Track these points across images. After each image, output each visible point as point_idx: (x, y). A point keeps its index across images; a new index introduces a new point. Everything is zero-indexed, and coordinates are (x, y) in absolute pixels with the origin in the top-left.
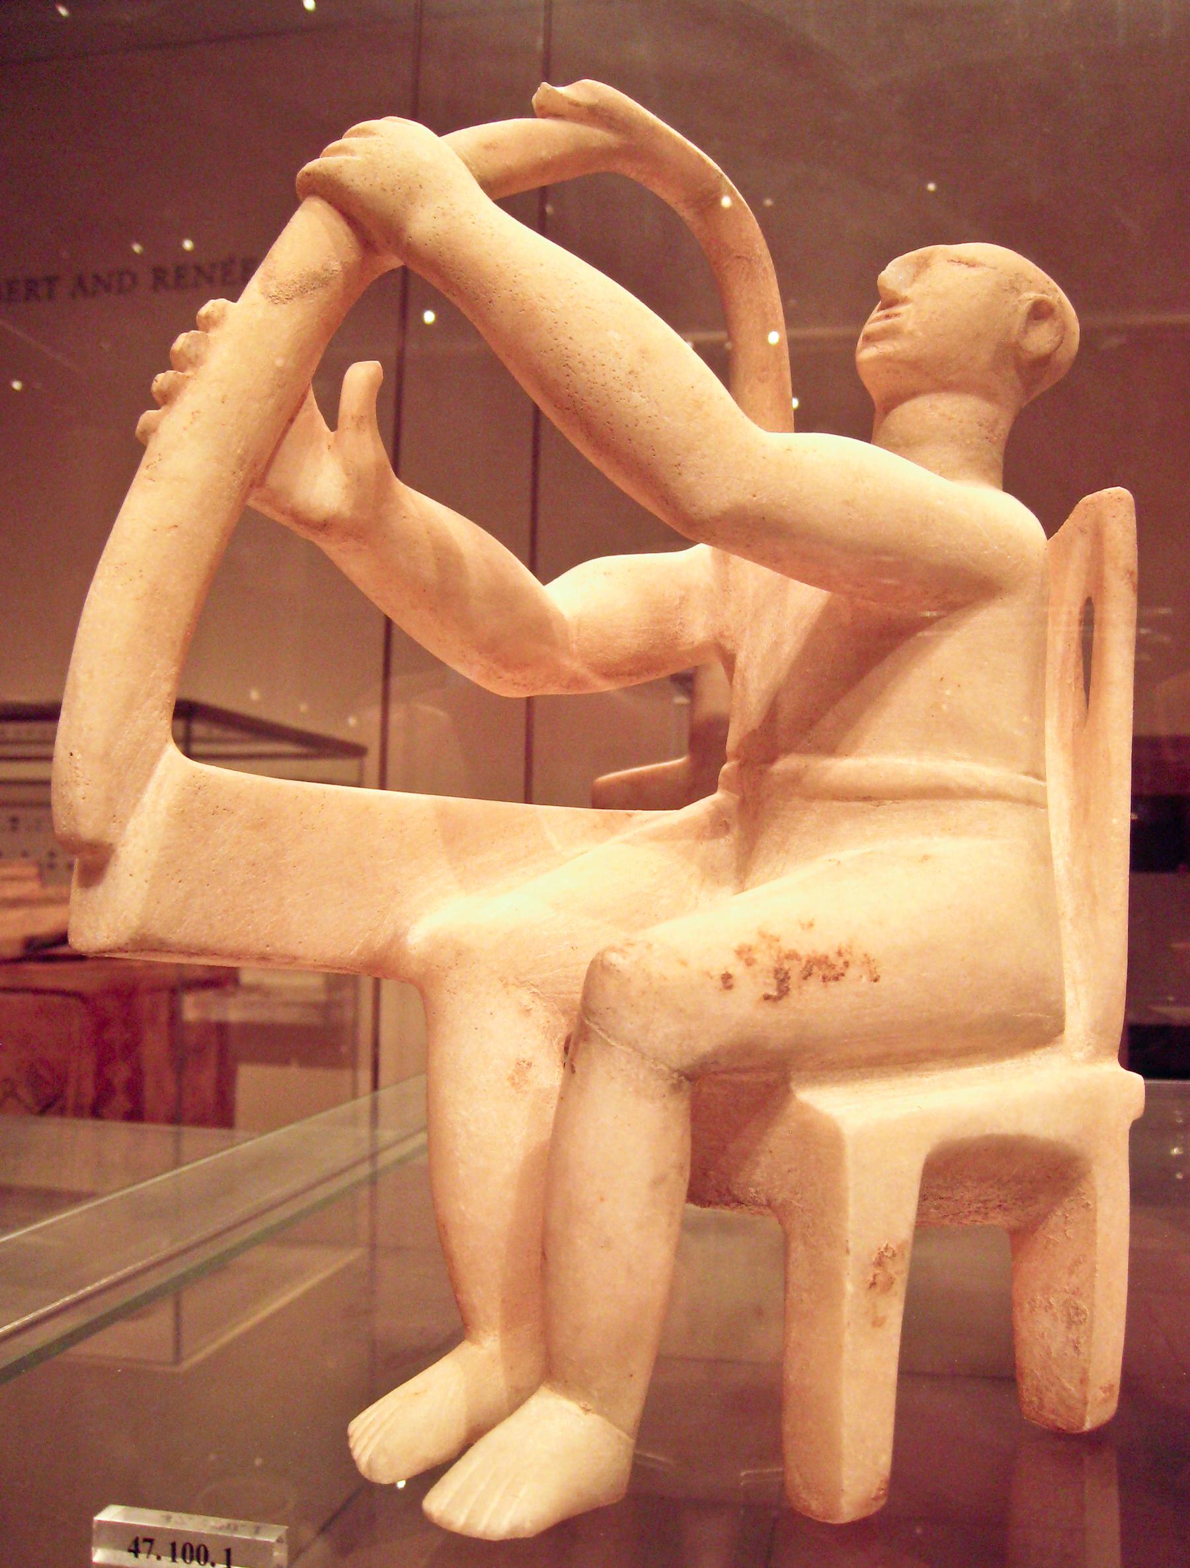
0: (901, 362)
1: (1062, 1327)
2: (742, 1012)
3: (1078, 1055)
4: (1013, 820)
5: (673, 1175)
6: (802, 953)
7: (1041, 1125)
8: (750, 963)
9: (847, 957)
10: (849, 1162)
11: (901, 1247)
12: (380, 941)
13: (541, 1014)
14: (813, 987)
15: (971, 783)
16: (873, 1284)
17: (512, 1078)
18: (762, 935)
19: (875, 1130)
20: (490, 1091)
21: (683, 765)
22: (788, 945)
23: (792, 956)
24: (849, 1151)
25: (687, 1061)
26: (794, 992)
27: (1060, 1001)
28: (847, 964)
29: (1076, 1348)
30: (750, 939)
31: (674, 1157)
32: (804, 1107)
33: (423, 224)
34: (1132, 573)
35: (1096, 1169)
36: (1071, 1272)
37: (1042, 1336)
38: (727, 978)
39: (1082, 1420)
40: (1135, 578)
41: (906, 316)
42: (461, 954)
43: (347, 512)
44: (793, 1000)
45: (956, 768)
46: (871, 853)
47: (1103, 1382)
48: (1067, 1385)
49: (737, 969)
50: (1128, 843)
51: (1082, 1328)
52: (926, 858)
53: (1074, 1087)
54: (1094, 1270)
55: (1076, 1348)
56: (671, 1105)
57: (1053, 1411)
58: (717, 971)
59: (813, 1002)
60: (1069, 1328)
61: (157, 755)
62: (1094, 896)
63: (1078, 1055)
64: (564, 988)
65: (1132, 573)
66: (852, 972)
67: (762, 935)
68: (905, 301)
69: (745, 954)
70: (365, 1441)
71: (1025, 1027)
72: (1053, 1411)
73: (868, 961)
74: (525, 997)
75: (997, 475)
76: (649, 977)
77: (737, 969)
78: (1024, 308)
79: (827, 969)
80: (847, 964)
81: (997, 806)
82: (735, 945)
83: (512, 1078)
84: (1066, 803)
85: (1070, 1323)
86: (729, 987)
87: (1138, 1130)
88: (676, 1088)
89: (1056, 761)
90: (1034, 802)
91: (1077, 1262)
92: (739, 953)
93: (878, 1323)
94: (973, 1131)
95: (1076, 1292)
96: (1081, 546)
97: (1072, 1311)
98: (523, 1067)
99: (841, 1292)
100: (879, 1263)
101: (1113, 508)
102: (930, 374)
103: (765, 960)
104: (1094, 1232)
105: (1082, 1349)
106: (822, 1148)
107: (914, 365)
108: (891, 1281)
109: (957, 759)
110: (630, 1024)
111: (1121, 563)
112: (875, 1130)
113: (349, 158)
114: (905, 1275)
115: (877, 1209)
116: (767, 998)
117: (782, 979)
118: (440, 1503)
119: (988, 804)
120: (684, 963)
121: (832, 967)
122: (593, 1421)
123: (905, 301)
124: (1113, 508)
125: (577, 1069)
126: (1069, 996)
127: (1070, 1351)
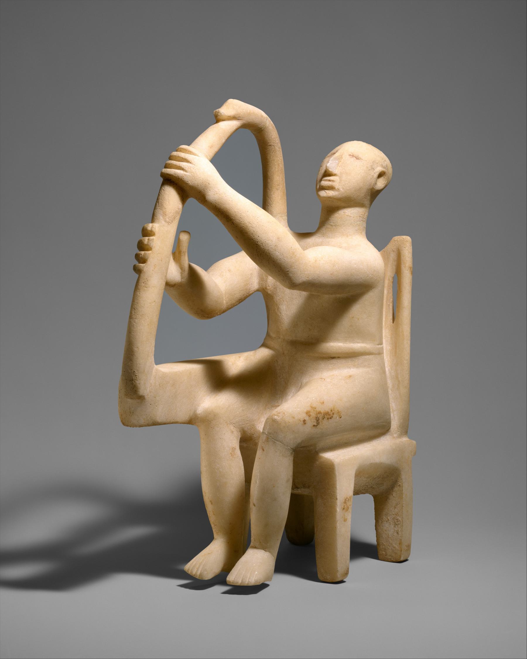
0: (335, 199)
1: (393, 526)
2: (308, 429)
3: (395, 435)
6: (322, 412)
7: (385, 459)
8: (309, 416)
9: (333, 412)
11: (350, 497)
16: (344, 509)
17: (231, 453)
18: (312, 407)
19: (346, 461)
21: (337, 340)
22: (318, 409)
23: (320, 413)
24: (336, 468)
26: (320, 423)
27: (390, 419)
28: (333, 414)
29: (397, 533)
30: (309, 409)
32: (322, 457)
35: (402, 473)
36: (395, 508)
37: (386, 531)
38: (304, 421)
39: (400, 557)
40: (412, 269)
41: (335, 182)
45: (357, 346)
46: (333, 375)
48: (395, 546)
49: (307, 418)
51: (399, 526)
52: (350, 376)
54: (403, 506)
55: (397, 533)
58: (302, 420)
59: (325, 424)
60: (395, 527)
62: (399, 381)
63: (395, 435)
64: (241, 423)
65: (411, 268)
66: (335, 416)
67: (312, 407)
68: (335, 175)
69: (308, 413)
71: (379, 428)
72: (390, 556)
73: (339, 412)
74: (232, 428)
75: (364, 233)
77: (307, 418)
78: (376, 175)
79: (328, 415)
80: (333, 414)
81: (371, 357)
82: (305, 411)
83: (231, 453)
84: (389, 348)
85: (395, 525)
86: (305, 424)
89: (386, 333)
90: (380, 353)
91: (397, 504)
92: (307, 413)
95: (397, 514)
96: (393, 256)
97: (396, 521)
99: (336, 511)
100: (345, 502)
101: (405, 243)
103: (313, 415)
104: (402, 494)
105: (400, 533)
107: (339, 199)
108: (348, 508)
109: (358, 343)
113: (185, 173)
116: (314, 426)
119: (367, 357)
121: (330, 415)
123: (335, 175)
125: (265, 449)
127: (395, 534)
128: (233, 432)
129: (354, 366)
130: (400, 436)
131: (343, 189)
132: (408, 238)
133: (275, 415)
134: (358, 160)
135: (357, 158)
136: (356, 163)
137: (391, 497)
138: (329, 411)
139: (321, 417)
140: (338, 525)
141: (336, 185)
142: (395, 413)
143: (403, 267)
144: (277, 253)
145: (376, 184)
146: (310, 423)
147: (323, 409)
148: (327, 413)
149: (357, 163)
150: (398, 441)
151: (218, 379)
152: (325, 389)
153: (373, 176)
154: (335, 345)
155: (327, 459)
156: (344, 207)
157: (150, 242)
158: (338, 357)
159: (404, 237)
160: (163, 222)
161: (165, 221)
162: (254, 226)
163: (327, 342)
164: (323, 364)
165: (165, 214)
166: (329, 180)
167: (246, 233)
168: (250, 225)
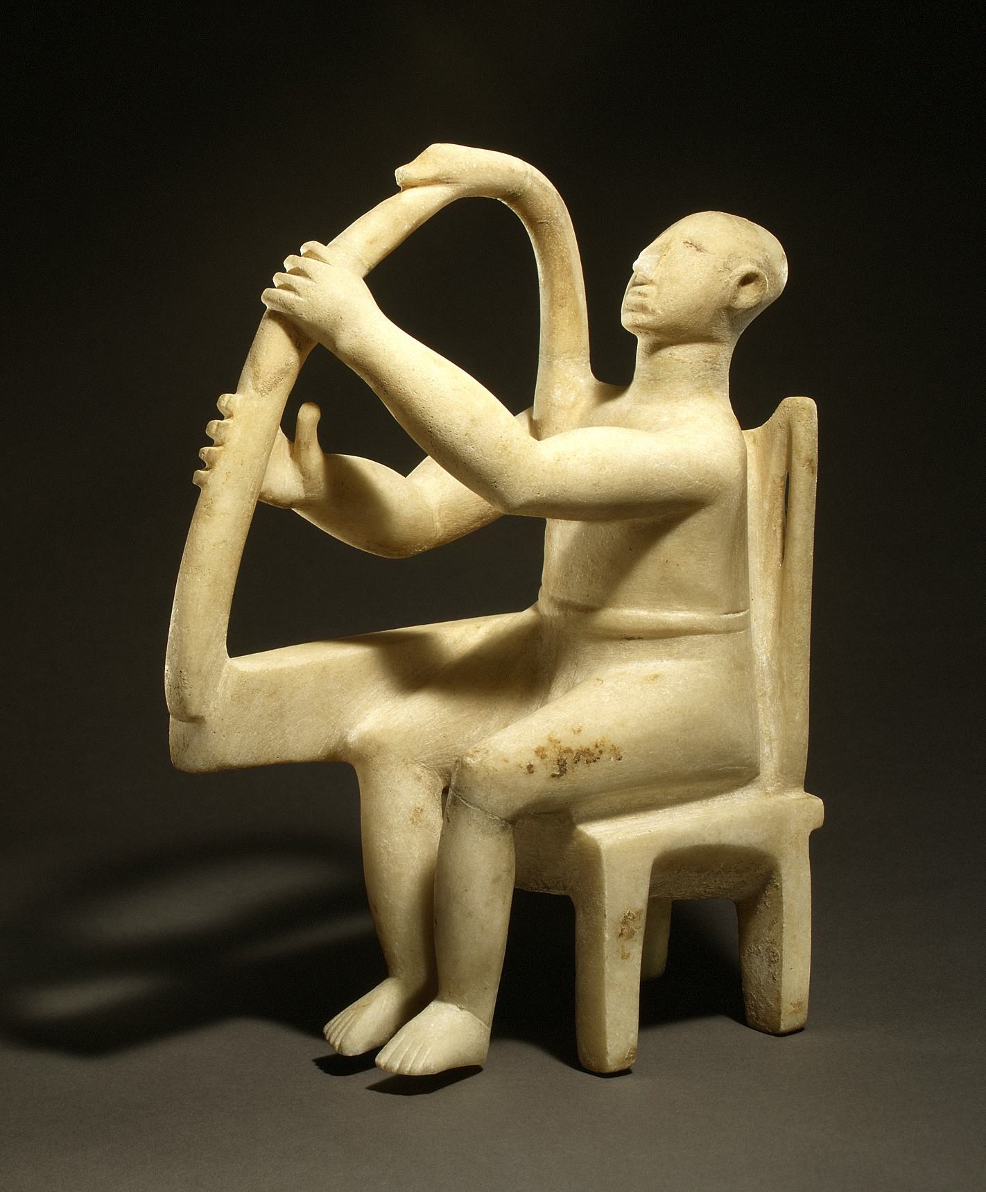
2: (540, 783)
4: (717, 647)
5: (504, 876)
8: (542, 757)
10: (605, 867)
12: (333, 743)
13: (427, 778)
14: (581, 767)
15: (686, 626)
18: (550, 740)
19: (626, 845)
20: (403, 831)
21: (636, 604)
22: (564, 745)
23: (568, 751)
24: (604, 858)
25: (509, 814)
26: (569, 771)
31: (504, 866)
32: (581, 833)
33: (347, 341)
34: (811, 461)
42: (381, 748)
43: (303, 495)
44: (569, 776)
45: (677, 616)
47: (794, 1000)
49: (536, 762)
50: (808, 647)
52: (656, 676)
53: (773, 811)
56: (502, 838)
57: (763, 1021)
58: (525, 764)
59: (581, 775)
61: (224, 662)
65: (811, 461)
66: (604, 756)
67: (550, 740)
69: (540, 753)
70: (334, 1035)
71: (726, 771)
72: (763, 1021)
74: (418, 770)
76: (487, 770)
77: (536, 762)
78: (734, 282)
79: (588, 756)
80: (601, 752)
81: (706, 637)
82: (535, 747)
87: (816, 838)
88: (504, 829)
90: (738, 629)
91: (773, 923)
93: (625, 956)
94: (687, 843)
96: (780, 436)
98: (418, 811)
99: (603, 939)
100: (625, 923)
101: (801, 412)
102: (671, 334)
103: (552, 754)
106: (590, 859)
110: (478, 795)
111: (803, 455)
112: (626, 845)
113: (297, 298)
114: (642, 930)
115: (623, 893)
116: (554, 776)
117: (562, 765)
118: (382, 1059)
120: (506, 761)
122: (465, 1015)
124: (801, 412)
126: (766, 750)
127: (770, 980)
128: (419, 778)
129: (671, 656)
130: (783, 789)
131: (663, 310)
132: (810, 403)
133: (468, 755)
134: (698, 254)
135: (699, 249)
136: (708, 257)
137: (761, 907)
138: (592, 748)
139: (565, 761)
140: (608, 967)
141: (650, 303)
142: (775, 744)
143: (794, 459)
144: (470, 449)
145: (735, 298)
146: (543, 772)
147: (576, 743)
148: (586, 752)
149: (698, 258)
150: (773, 801)
151: (417, 672)
152: (611, 701)
153: (728, 283)
154: (630, 613)
155: (589, 838)
156: (672, 344)
157: (221, 430)
158: (640, 638)
159: (799, 399)
160: (252, 392)
161: (256, 389)
162: (424, 397)
163: (619, 608)
164: (611, 649)
165: (256, 377)
166: (640, 294)
167: (410, 410)
168: (415, 396)
